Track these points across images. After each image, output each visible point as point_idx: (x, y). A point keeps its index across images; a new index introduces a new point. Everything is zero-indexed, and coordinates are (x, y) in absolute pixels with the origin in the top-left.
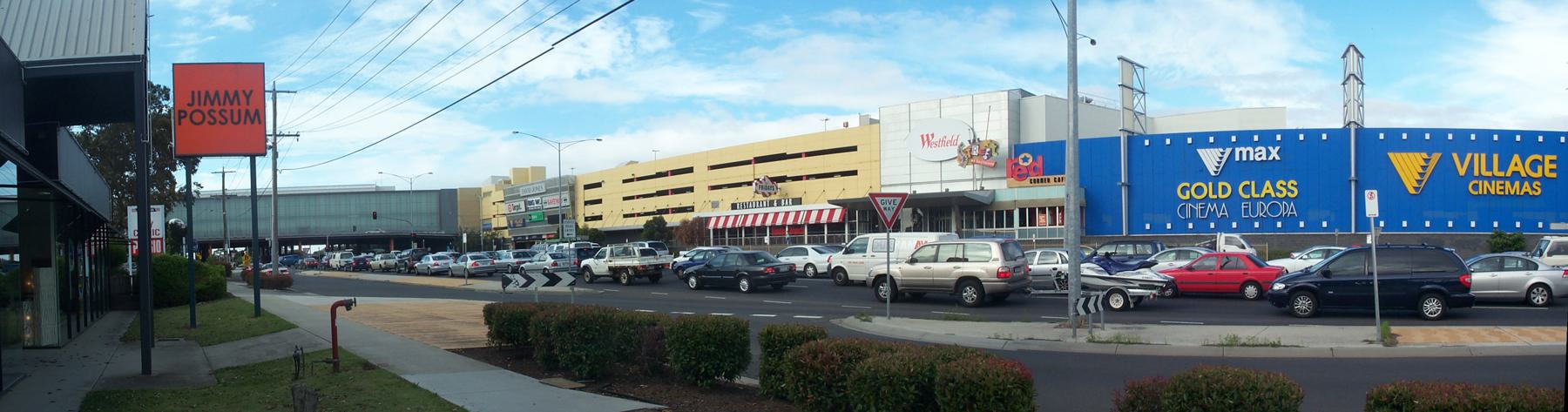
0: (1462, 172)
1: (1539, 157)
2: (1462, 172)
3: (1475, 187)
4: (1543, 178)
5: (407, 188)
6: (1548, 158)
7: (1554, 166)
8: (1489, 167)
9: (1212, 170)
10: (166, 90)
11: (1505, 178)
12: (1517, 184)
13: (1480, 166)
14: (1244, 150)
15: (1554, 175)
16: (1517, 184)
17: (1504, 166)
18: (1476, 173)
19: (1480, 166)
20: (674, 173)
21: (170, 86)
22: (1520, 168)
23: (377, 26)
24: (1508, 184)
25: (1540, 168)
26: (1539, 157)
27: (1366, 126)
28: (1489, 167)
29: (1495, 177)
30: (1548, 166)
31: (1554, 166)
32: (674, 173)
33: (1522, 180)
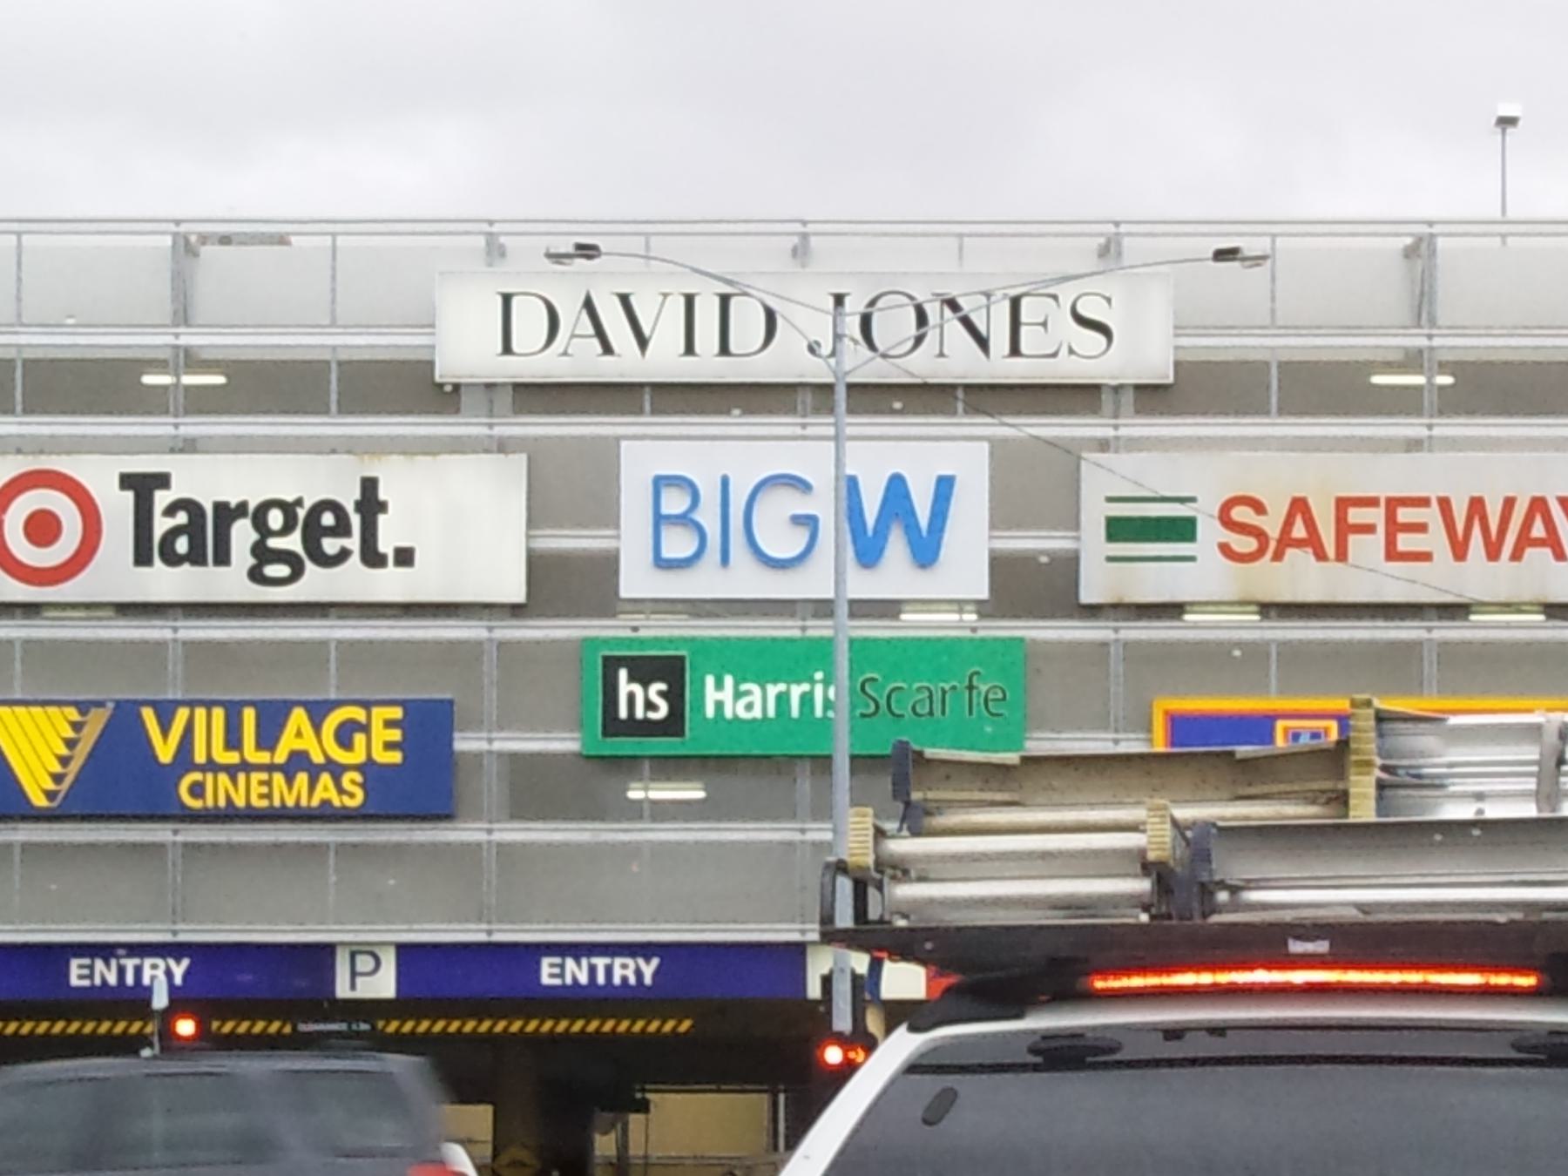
0: (165, 752)
1: (359, 714)
2: (165, 752)
3: (197, 790)
4: (368, 768)
5: (241, 456)
6: (380, 714)
7: (395, 735)
8: (233, 740)
9: (36, 786)
10: (1346, 816)
11: (270, 768)
12: (302, 779)
13: (210, 740)
14: (796, 691)
15: (395, 757)
16: (302, 779)
17: (268, 738)
18: (200, 757)
19: (210, 740)
20: (845, 234)
21: (1351, 820)
22: (308, 743)
23: (153, 978)
24: (278, 778)
25: (359, 739)
26: (359, 714)
27: (984, 594)
28: (233, 740)
29: (246, 767)
30: (381, 735)
31: (395, 735)
32: (845, 234)
33: (314, 772)
